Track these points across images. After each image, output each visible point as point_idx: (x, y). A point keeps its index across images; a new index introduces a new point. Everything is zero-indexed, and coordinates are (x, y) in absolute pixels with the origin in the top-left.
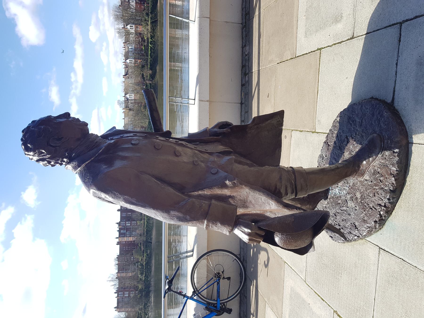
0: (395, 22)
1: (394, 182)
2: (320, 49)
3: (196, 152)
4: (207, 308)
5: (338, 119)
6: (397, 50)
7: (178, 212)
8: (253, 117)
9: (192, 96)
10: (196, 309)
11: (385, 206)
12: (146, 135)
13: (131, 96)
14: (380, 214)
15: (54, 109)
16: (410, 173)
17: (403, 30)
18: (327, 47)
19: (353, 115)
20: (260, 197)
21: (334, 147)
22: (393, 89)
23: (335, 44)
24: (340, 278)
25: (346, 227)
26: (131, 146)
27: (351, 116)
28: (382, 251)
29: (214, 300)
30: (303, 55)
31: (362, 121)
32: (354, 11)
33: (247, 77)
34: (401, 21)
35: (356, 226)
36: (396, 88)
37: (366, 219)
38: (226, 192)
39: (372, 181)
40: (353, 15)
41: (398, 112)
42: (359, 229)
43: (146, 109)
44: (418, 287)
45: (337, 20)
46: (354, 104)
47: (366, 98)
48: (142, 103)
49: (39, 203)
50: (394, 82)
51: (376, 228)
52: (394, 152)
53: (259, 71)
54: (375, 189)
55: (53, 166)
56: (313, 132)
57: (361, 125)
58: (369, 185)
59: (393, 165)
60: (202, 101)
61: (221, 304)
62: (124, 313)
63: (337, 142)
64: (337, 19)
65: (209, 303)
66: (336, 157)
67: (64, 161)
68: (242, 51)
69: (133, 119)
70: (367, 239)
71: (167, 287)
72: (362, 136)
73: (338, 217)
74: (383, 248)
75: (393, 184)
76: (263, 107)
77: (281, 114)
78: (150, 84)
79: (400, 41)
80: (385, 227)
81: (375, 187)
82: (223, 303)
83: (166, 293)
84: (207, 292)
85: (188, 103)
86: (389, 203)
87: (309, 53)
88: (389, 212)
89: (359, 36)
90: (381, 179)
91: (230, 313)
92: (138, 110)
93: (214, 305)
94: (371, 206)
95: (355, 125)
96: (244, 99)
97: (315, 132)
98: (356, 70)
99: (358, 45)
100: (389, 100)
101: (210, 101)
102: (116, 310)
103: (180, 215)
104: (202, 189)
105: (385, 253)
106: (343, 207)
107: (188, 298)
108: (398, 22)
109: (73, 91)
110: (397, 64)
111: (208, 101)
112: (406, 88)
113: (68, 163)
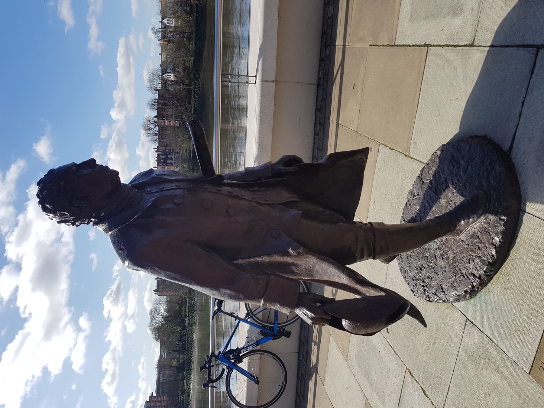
0: (531, 43)
1: (495, 255)
2: (428, 46)
3: (254, 204)
4: (262, 332)
5: (439, 153)
6: (527, 84)
7: (230, 290)
8: (328, 154)
9: (252, 72)
10: (249, 331)
11: (480, 278)
12: (192, 185)
13: (171, 22)
14: (472, 285)
15: (66, 31)
16: (515, 246)
17: (539, 57)
18: (437, 46)
19: (458, 154)
20: (330, 268)
21: (430, 188)
22: (512, 136)
23: (448, 46)
24: (417, 336)
25: (431, 287)
26: (173, 206)
27: (456, 155)
28: (468, 323)
29: (271, 323)
30: (405, 45)
31: (467, 167)
32: (479, 7)
33: (327, 49)
34: (539, 44)
35: (442, 289)
36: (517, 134)
37: (455, 284)
38: (288, 259)
39: (468, 245)
40: (478, 12)
41: (514, 167)
42: (446, 293)
43: (190, 41)
44: (503, 373)
45: (454, 12)
46: (462, 140)
47: (477, 134)
48: (185, 32)
49: (56, 158)
50: (515, 125)
51: (465, 298)
52: (500, 219)
53: (344, 46)
54: (471, 255)
55: (77, 226)
56: (406, 156)
57: (466, 172)
58: (465, 248)
59: (497, 234)
60: (266, 81)
61: (279, 327)
62: (165, 297)
63: (433, 182)
64: (456, 11)
65: (264, 327)
66: (429, 200)
67: (92, 221)
68: (324, 11)
69: (173, 56)
70: (454, 303)
71: (216, 308)
72: (465, 186)
73: (423, 272)
74: (470, 319)
75: (493, 256)
76: (341, 142)
77: (365, 151)
78: (196, 4)
79: (532, 72)
80: (477, 298)
81: (471, 253)
82: (282, 327)
83: (215, 313)
84: (263, 315)
85: (247, 82)
86: (485, 275)
87: (413, 46)
88: (484, 283)
89: (481, 46)
90: (480, 245)
91: (288, 337)
92: (180, 43)
93: (271, 329)
94: (464, 272)
95: (458, 168)
96: (322, 79)
97: (408, 156)
98: (470, 92)
99: (478, 58)
100: (506, 148)
101: (276, 82)
102: (155, 294)
103: (231, 293)
104: (259, 256)
105: (472, 326)
106: (430, 262)
107: (240, 320)
108: (535, 44)
109: (91, 8)
110: (523, 103)
111: (273, 82)
112: (529, 139)
113: (95, 224)
